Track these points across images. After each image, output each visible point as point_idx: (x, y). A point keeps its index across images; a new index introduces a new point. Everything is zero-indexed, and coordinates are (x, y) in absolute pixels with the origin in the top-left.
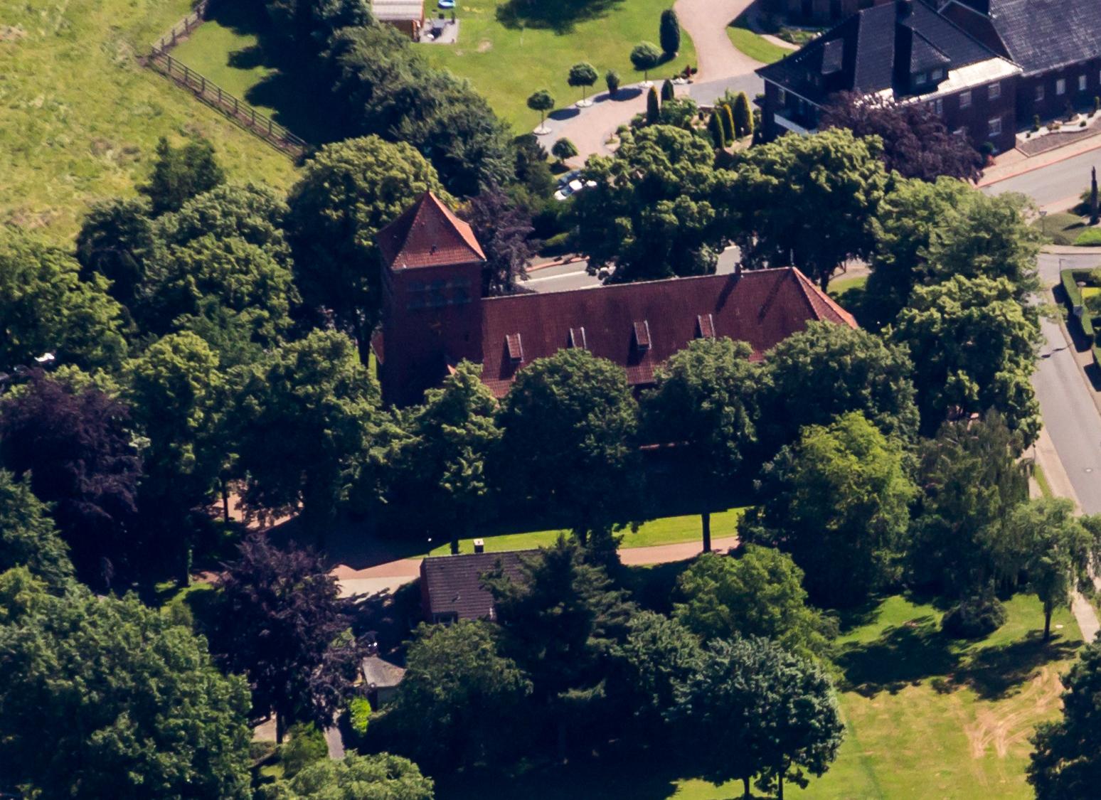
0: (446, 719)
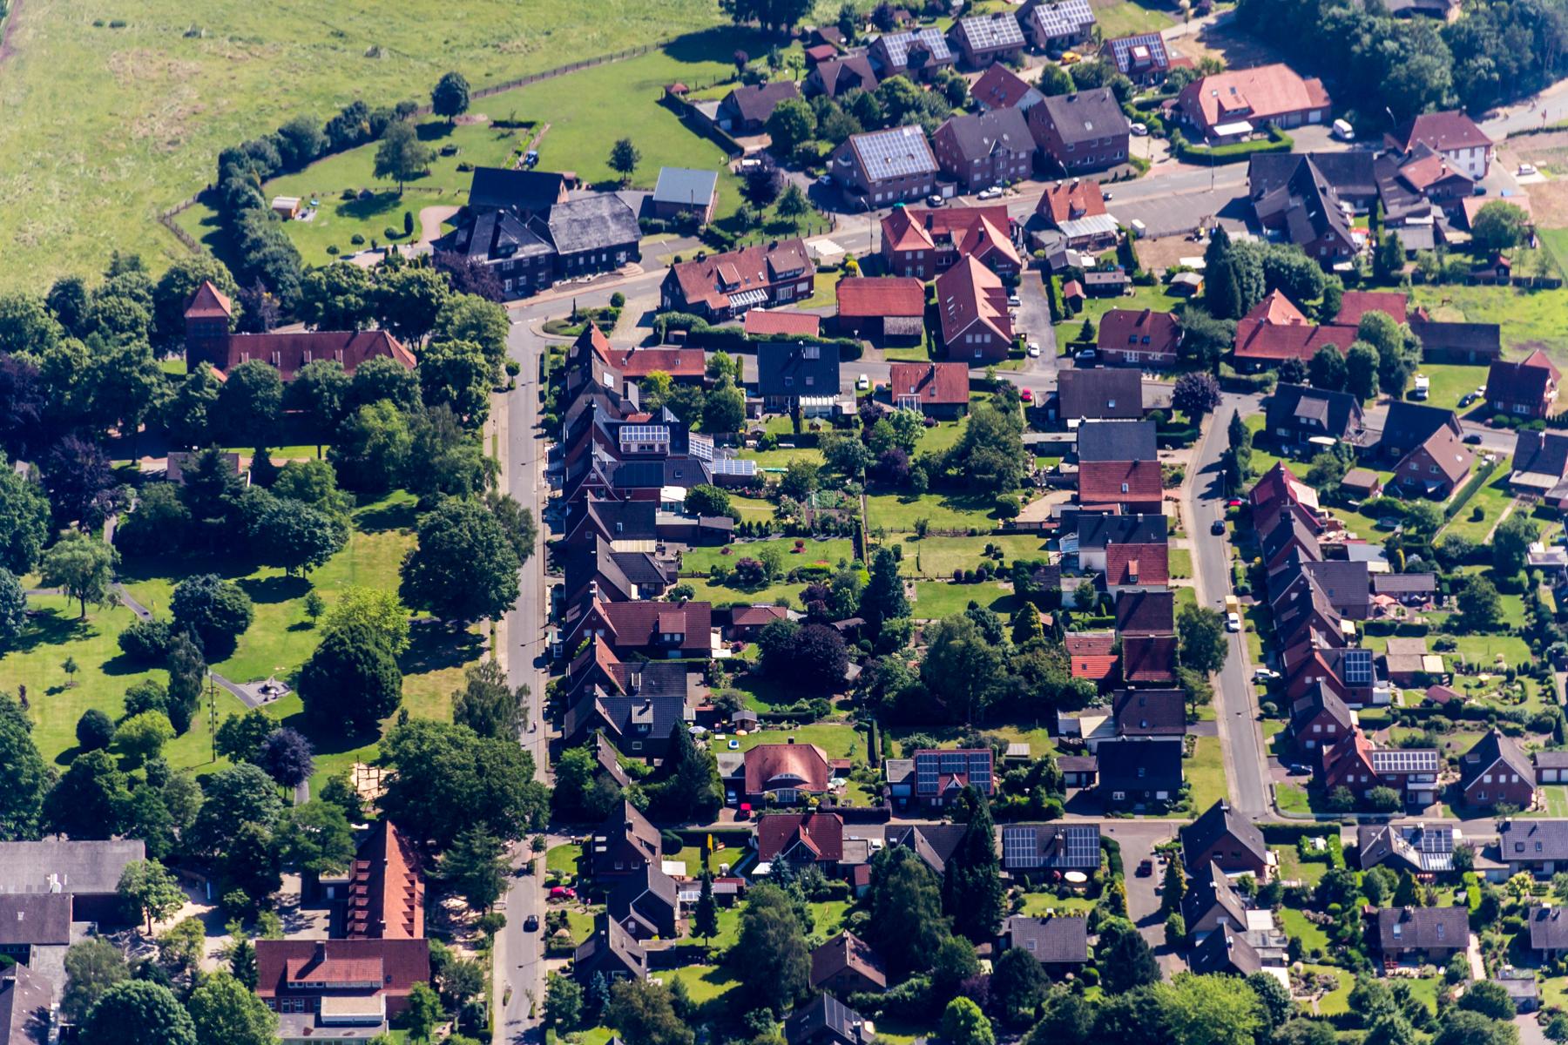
0: (149, 528)
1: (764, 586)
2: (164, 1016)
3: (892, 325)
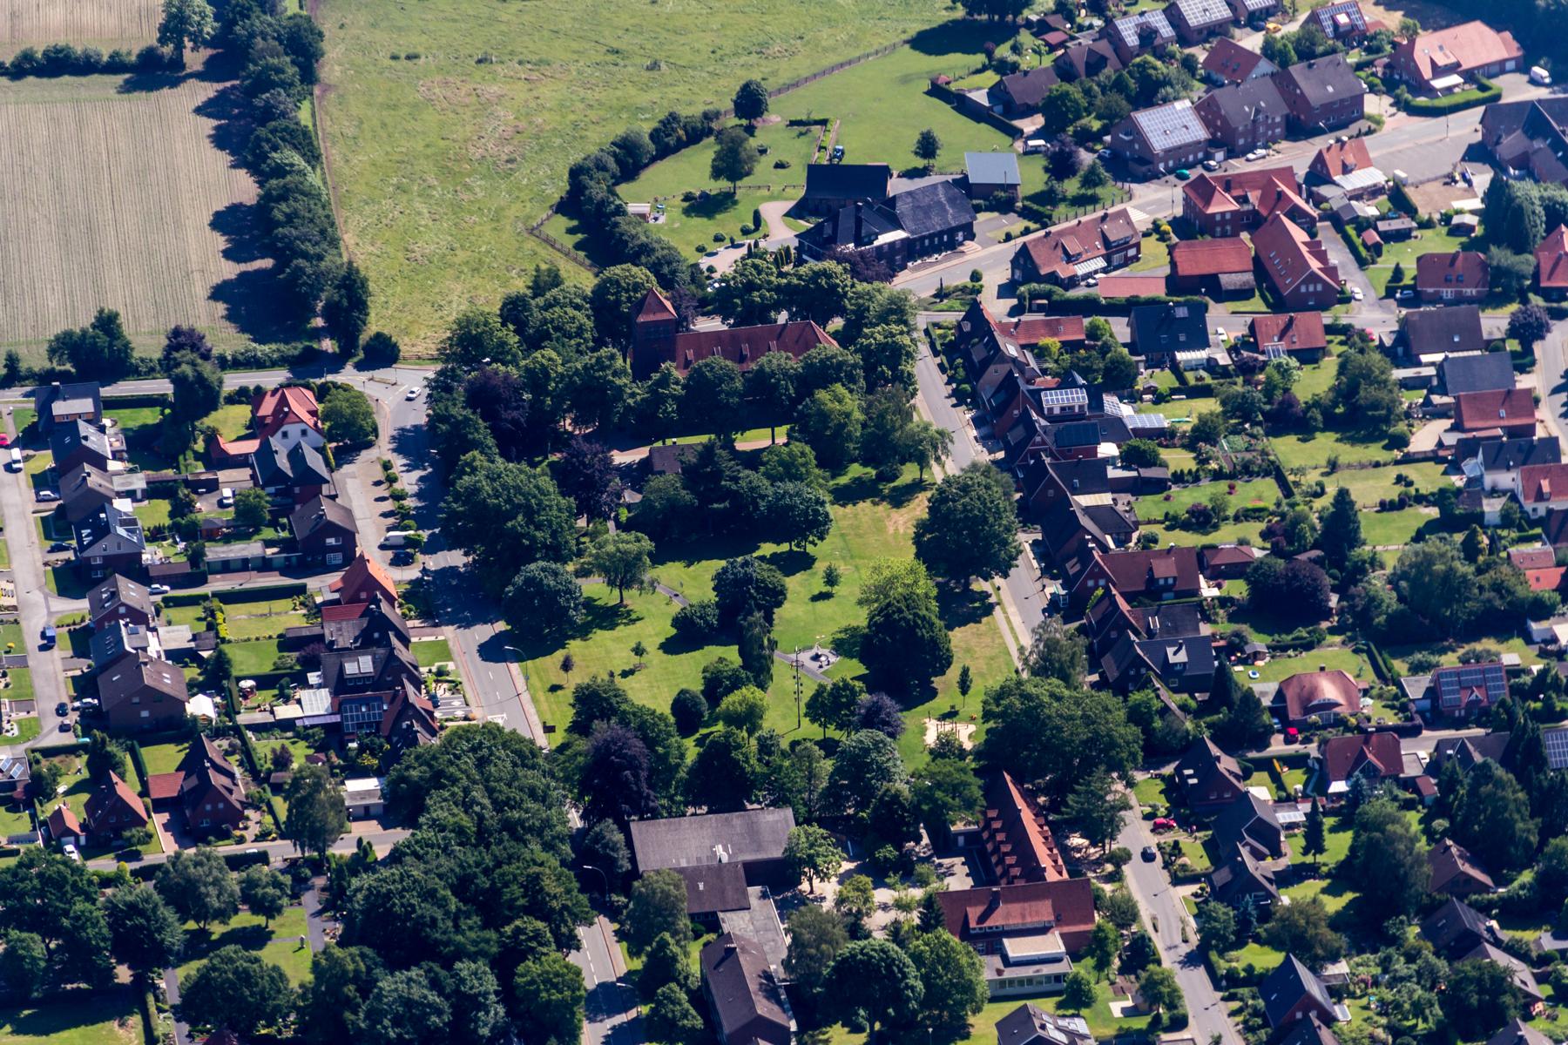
1: (1216, 527)
2: (900, 970)
3: (1228, 281)
